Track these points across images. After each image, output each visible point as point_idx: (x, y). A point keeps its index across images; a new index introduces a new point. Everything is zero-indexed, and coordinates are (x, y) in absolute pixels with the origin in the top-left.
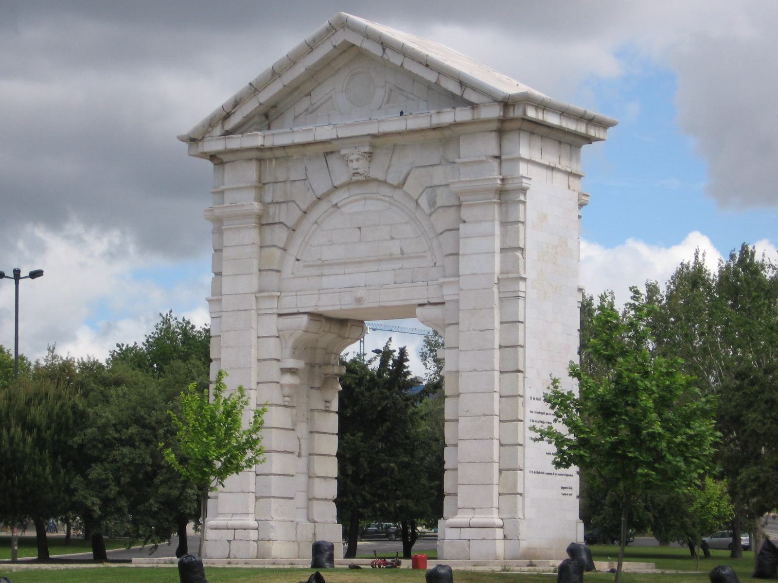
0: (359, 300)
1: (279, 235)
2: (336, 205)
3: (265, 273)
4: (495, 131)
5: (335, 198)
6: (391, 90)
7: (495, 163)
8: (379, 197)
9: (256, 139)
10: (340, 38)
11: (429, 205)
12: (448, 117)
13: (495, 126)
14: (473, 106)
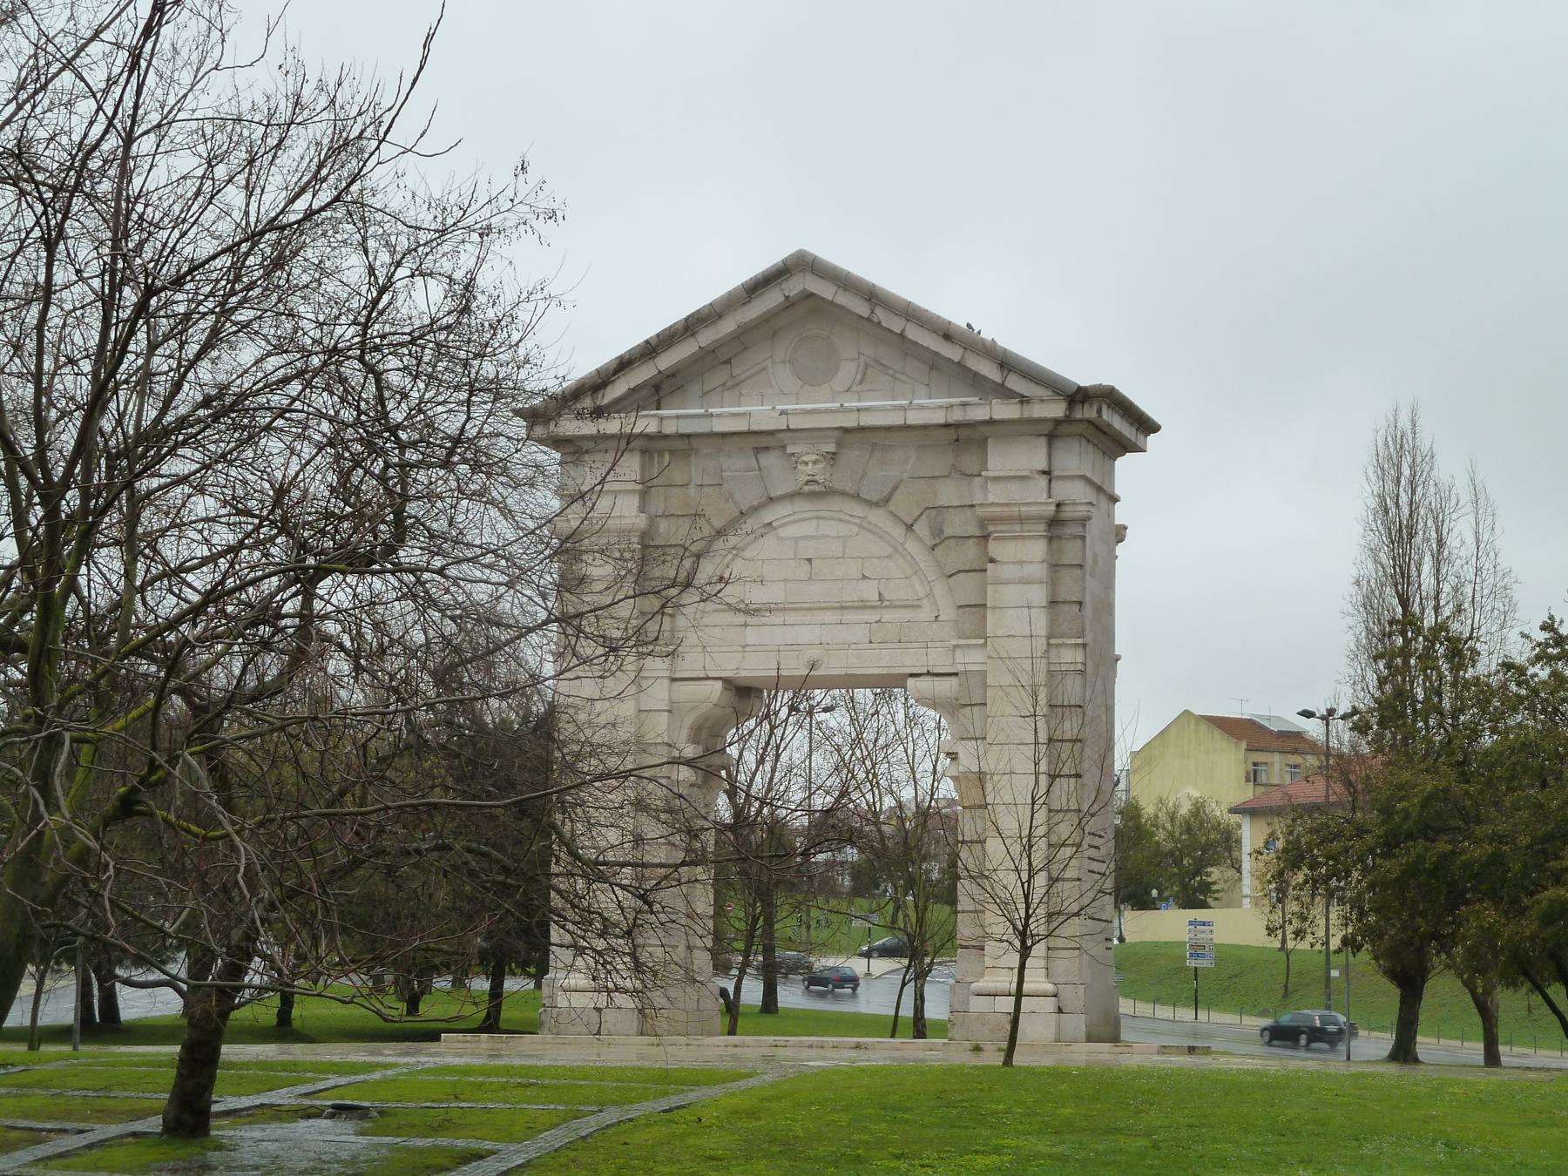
2: (770, 524)
5: (768, 516)
6: (867, 366)
7: (1042, 482)
9: (646, 423)
10: (795, 286)
11: (932, 534)
13: (1047, 428)
14: (1024, 400)
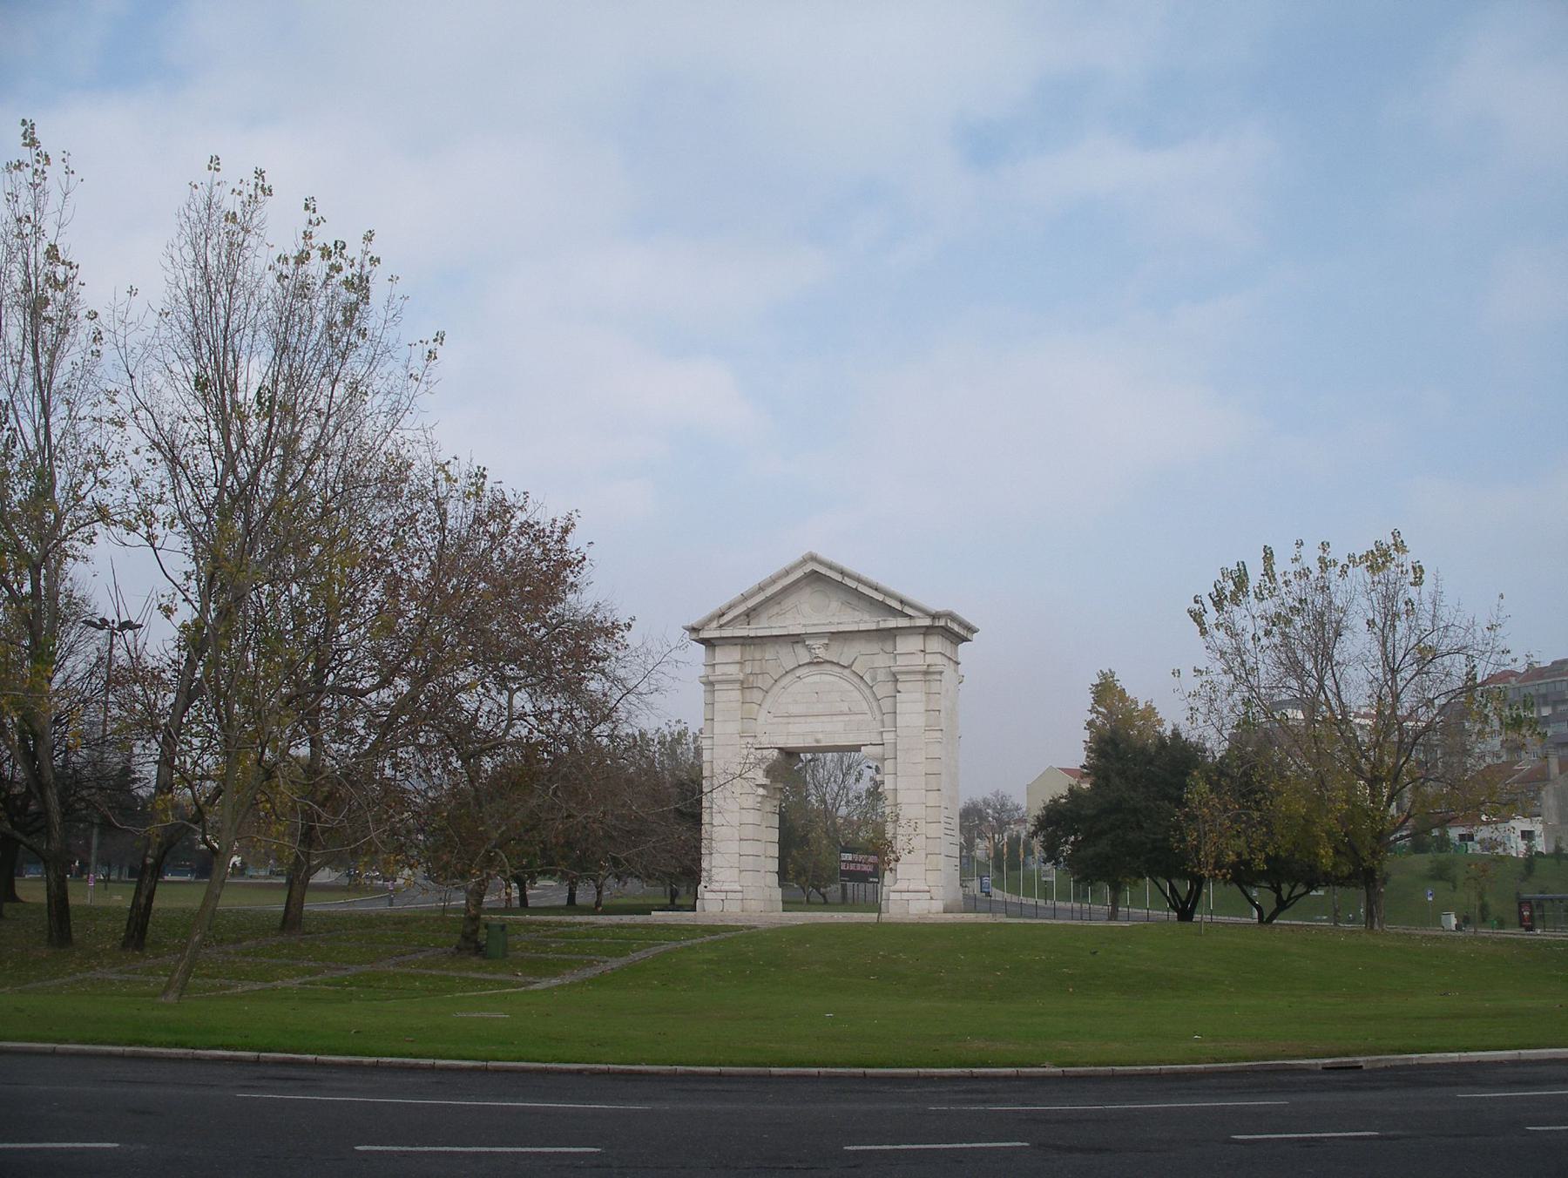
0: (817, 741)
1: (756, 695)
3: (745, 720)
5: (799, 673)
12: (892, 623)
13: (923, 631)
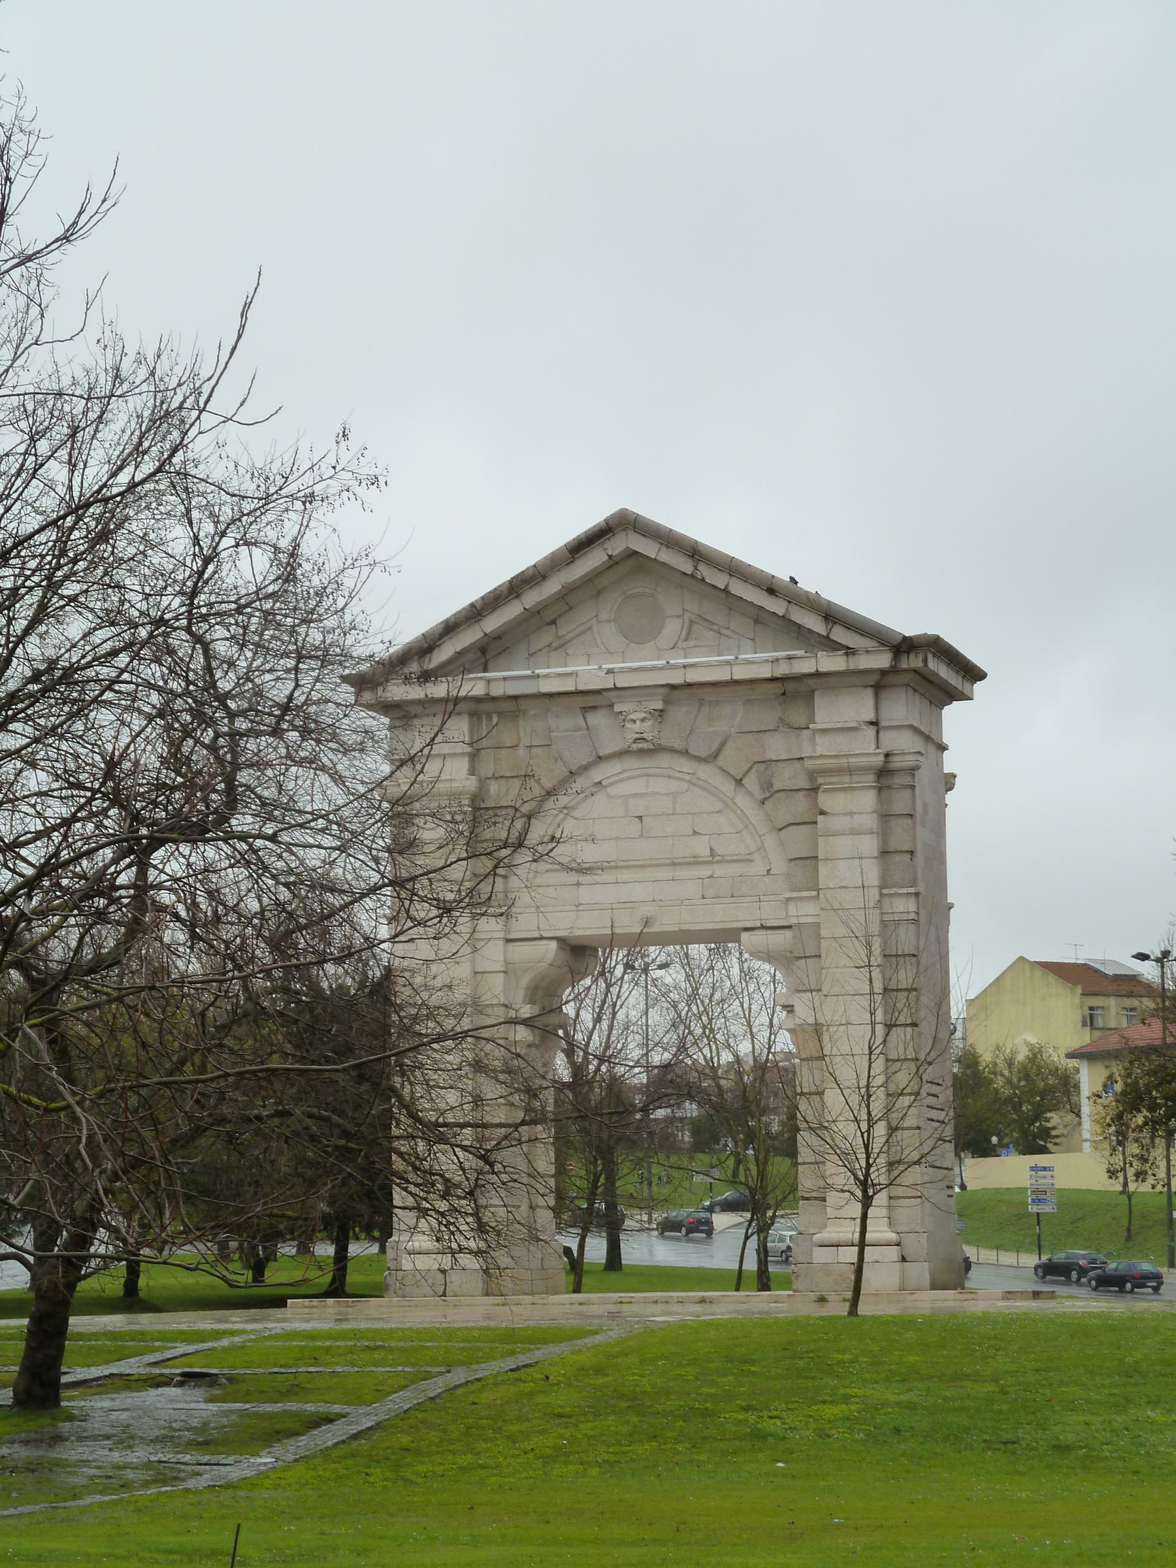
2: (600, 783)
4: (871, 686)
5: (597, 774)
6: (692, 622)
7: (870, 732)
8: (672, 773)
9: (473, 686)
10: (618, 545)
14: (849, 651)
